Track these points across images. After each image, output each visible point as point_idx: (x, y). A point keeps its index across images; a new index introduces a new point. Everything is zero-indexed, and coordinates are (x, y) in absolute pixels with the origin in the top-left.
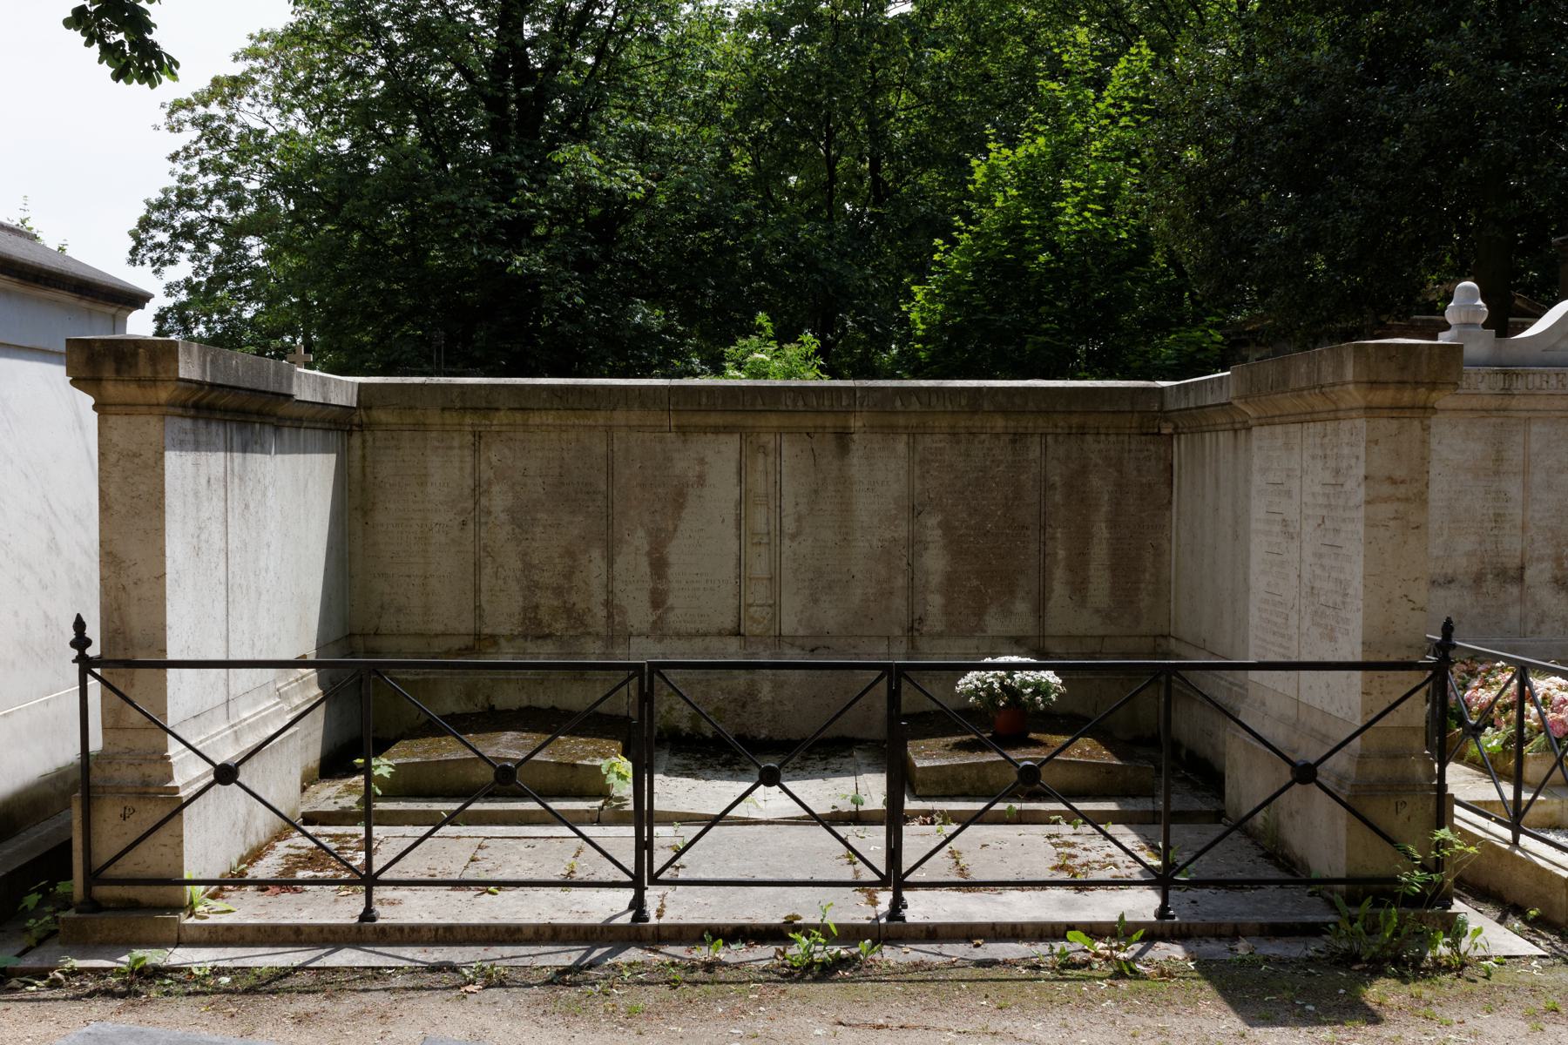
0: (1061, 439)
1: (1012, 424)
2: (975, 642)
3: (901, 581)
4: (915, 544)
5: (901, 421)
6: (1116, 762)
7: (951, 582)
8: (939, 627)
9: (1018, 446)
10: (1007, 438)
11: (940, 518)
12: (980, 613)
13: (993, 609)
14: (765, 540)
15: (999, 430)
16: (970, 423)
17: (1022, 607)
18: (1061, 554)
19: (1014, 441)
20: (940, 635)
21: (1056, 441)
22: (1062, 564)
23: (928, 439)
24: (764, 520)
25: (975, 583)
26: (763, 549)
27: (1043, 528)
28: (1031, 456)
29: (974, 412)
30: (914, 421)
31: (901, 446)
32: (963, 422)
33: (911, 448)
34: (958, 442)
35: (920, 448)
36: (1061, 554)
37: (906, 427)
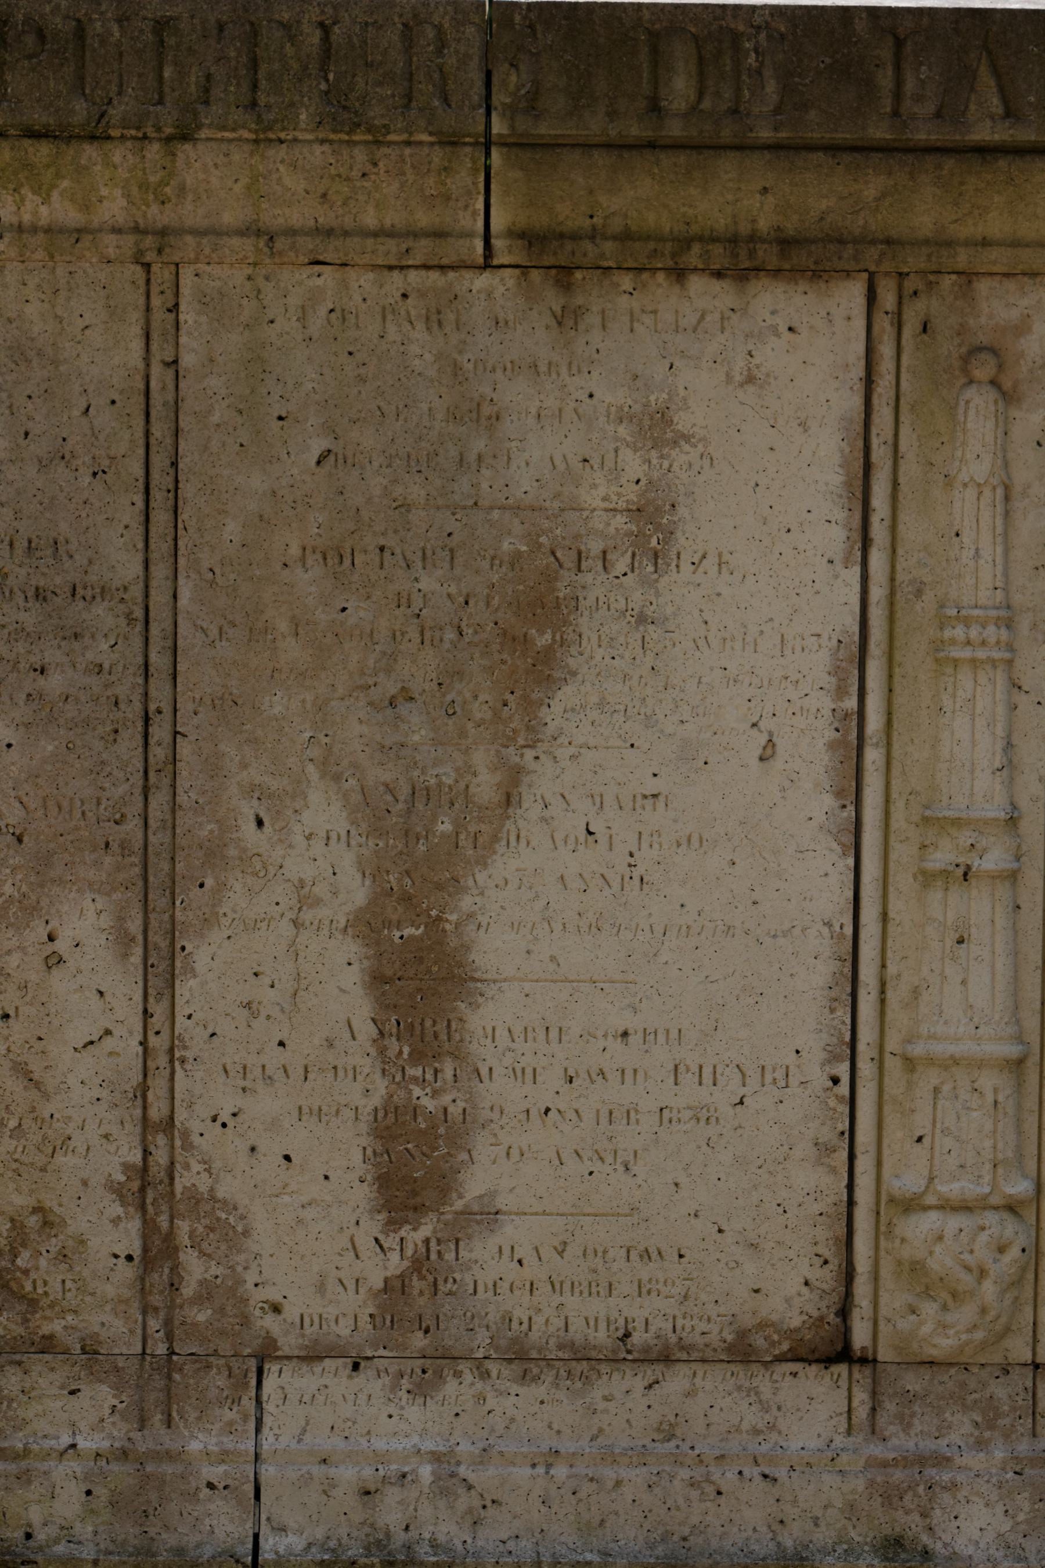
14: (994, 859)
24: (987, 750)
26: (981, 907)
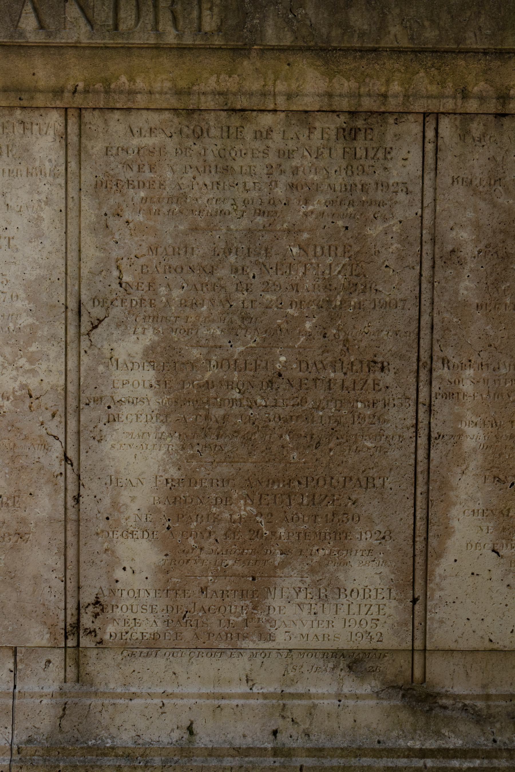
0: (476, 128)
1: (344, 85)
2: (241, 664)
3: (45, 505)
4: (81, 406)
5: (42, 72)
6: (271, 22)
7: (179, 510)
8: (148, 625)
9: (360, 144)
10: (332, 124)
11: (149, 337)
12: (256, 587)
13: (290, 580)
15: (309, 102)
16: (230, 83)
17: (367, 574)
18: (474, 436)
19: (350, 134)
20: (152, 646)
21: (464, 134)
22: (474, 464)
23: (117, 124)
25: (243, 509)
27: (424, 368)
28: (397, 174)
29: (240, 51)
30: (77, 74)
31: (44, 142)
32: (212, 79)
33: (73, 147)
34: (199, 135)
35: (96, 147)
36: (474, 436)
37: (58, 92)
